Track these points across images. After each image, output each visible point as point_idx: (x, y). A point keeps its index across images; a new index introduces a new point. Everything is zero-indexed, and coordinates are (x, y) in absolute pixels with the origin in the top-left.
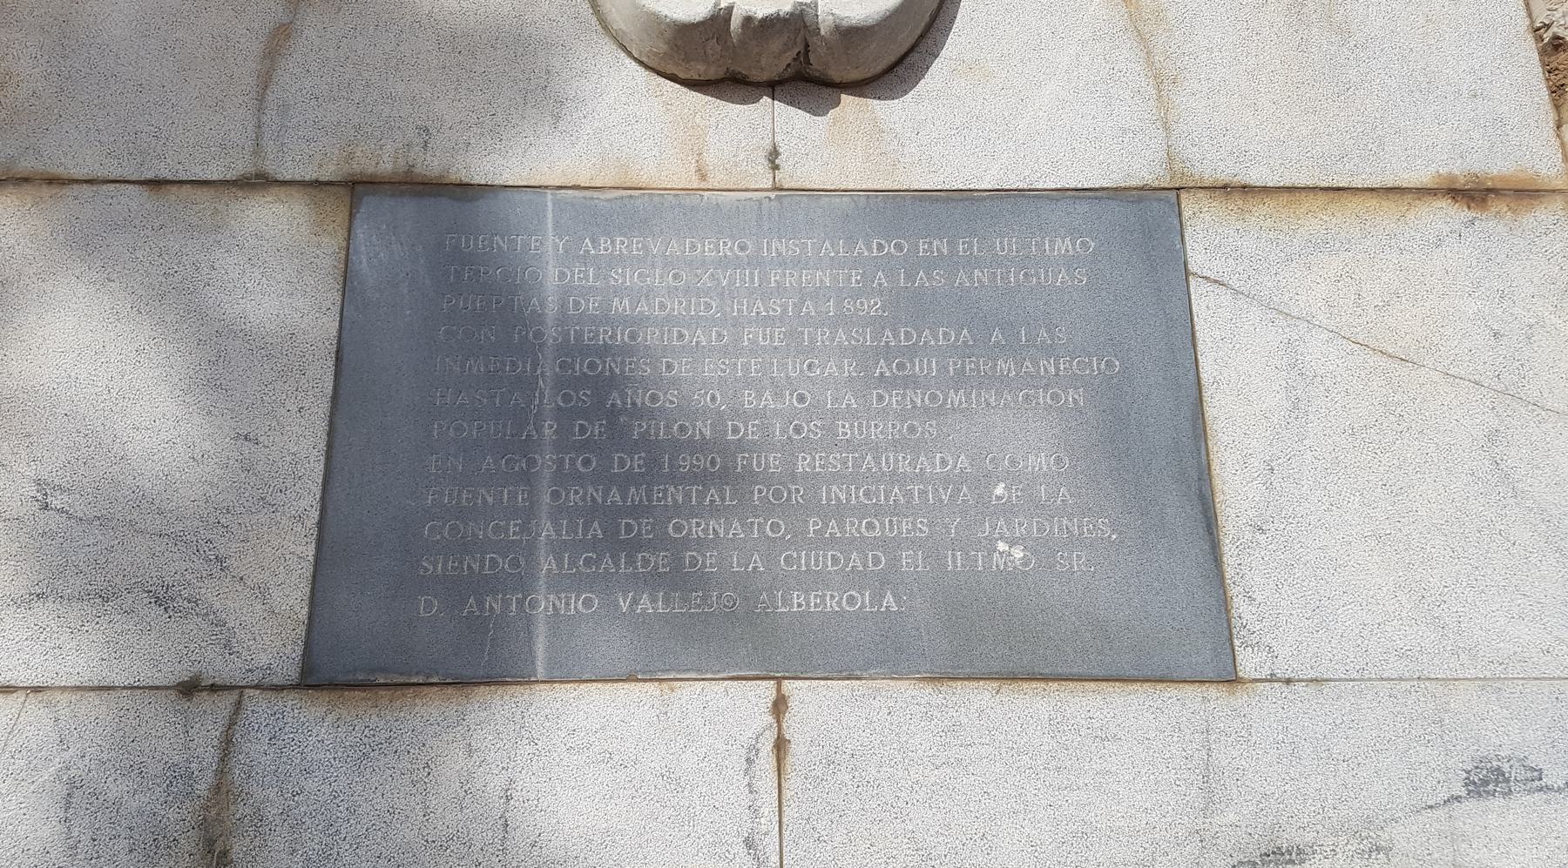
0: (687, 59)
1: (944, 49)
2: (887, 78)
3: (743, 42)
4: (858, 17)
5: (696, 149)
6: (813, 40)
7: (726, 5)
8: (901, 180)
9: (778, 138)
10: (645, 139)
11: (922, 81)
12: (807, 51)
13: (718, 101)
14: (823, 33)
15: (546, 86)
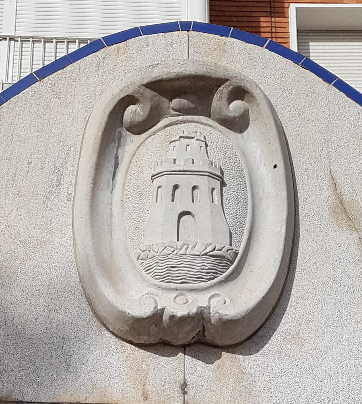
0: (139, 334)
1: (280, 326)
2: (247, 343)
3: (169, 327)
4: (232, 315)
5: (142, 382)
6: (207, 325)
7: (161, 308)
8: (253, 401)
9: (187, 376)
10: (115, 376)
11: (267, 345)
12: (204, 331)
13: (155, 355)
14: (213, 322)
15: (63, 347)
